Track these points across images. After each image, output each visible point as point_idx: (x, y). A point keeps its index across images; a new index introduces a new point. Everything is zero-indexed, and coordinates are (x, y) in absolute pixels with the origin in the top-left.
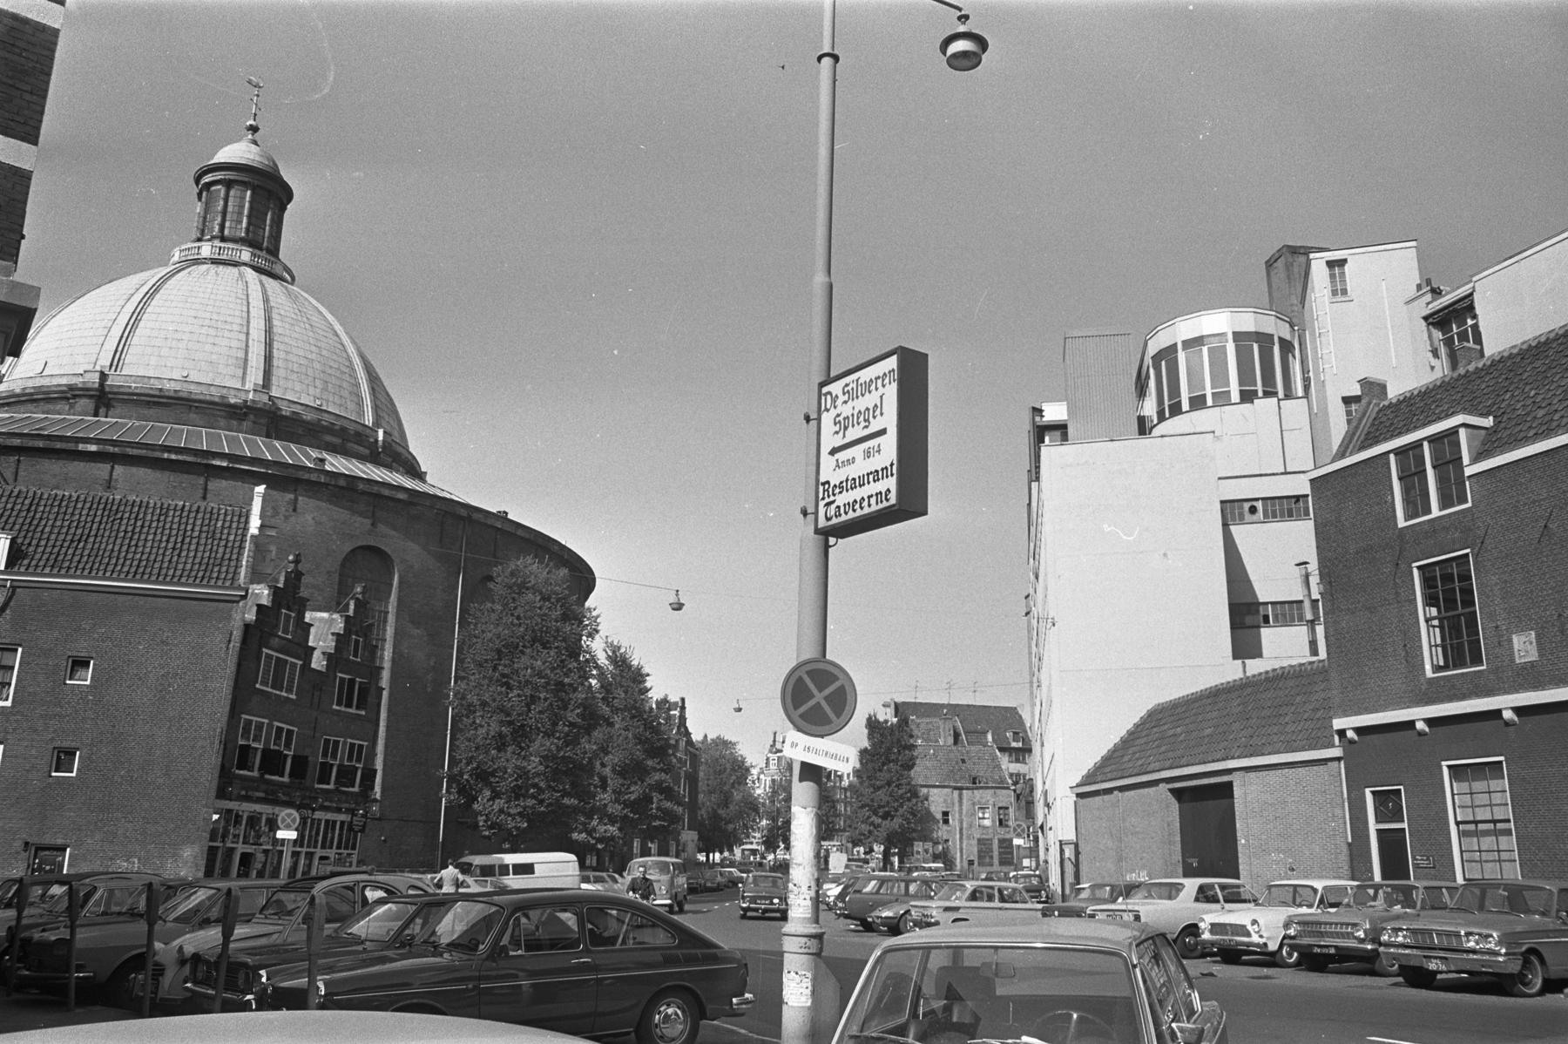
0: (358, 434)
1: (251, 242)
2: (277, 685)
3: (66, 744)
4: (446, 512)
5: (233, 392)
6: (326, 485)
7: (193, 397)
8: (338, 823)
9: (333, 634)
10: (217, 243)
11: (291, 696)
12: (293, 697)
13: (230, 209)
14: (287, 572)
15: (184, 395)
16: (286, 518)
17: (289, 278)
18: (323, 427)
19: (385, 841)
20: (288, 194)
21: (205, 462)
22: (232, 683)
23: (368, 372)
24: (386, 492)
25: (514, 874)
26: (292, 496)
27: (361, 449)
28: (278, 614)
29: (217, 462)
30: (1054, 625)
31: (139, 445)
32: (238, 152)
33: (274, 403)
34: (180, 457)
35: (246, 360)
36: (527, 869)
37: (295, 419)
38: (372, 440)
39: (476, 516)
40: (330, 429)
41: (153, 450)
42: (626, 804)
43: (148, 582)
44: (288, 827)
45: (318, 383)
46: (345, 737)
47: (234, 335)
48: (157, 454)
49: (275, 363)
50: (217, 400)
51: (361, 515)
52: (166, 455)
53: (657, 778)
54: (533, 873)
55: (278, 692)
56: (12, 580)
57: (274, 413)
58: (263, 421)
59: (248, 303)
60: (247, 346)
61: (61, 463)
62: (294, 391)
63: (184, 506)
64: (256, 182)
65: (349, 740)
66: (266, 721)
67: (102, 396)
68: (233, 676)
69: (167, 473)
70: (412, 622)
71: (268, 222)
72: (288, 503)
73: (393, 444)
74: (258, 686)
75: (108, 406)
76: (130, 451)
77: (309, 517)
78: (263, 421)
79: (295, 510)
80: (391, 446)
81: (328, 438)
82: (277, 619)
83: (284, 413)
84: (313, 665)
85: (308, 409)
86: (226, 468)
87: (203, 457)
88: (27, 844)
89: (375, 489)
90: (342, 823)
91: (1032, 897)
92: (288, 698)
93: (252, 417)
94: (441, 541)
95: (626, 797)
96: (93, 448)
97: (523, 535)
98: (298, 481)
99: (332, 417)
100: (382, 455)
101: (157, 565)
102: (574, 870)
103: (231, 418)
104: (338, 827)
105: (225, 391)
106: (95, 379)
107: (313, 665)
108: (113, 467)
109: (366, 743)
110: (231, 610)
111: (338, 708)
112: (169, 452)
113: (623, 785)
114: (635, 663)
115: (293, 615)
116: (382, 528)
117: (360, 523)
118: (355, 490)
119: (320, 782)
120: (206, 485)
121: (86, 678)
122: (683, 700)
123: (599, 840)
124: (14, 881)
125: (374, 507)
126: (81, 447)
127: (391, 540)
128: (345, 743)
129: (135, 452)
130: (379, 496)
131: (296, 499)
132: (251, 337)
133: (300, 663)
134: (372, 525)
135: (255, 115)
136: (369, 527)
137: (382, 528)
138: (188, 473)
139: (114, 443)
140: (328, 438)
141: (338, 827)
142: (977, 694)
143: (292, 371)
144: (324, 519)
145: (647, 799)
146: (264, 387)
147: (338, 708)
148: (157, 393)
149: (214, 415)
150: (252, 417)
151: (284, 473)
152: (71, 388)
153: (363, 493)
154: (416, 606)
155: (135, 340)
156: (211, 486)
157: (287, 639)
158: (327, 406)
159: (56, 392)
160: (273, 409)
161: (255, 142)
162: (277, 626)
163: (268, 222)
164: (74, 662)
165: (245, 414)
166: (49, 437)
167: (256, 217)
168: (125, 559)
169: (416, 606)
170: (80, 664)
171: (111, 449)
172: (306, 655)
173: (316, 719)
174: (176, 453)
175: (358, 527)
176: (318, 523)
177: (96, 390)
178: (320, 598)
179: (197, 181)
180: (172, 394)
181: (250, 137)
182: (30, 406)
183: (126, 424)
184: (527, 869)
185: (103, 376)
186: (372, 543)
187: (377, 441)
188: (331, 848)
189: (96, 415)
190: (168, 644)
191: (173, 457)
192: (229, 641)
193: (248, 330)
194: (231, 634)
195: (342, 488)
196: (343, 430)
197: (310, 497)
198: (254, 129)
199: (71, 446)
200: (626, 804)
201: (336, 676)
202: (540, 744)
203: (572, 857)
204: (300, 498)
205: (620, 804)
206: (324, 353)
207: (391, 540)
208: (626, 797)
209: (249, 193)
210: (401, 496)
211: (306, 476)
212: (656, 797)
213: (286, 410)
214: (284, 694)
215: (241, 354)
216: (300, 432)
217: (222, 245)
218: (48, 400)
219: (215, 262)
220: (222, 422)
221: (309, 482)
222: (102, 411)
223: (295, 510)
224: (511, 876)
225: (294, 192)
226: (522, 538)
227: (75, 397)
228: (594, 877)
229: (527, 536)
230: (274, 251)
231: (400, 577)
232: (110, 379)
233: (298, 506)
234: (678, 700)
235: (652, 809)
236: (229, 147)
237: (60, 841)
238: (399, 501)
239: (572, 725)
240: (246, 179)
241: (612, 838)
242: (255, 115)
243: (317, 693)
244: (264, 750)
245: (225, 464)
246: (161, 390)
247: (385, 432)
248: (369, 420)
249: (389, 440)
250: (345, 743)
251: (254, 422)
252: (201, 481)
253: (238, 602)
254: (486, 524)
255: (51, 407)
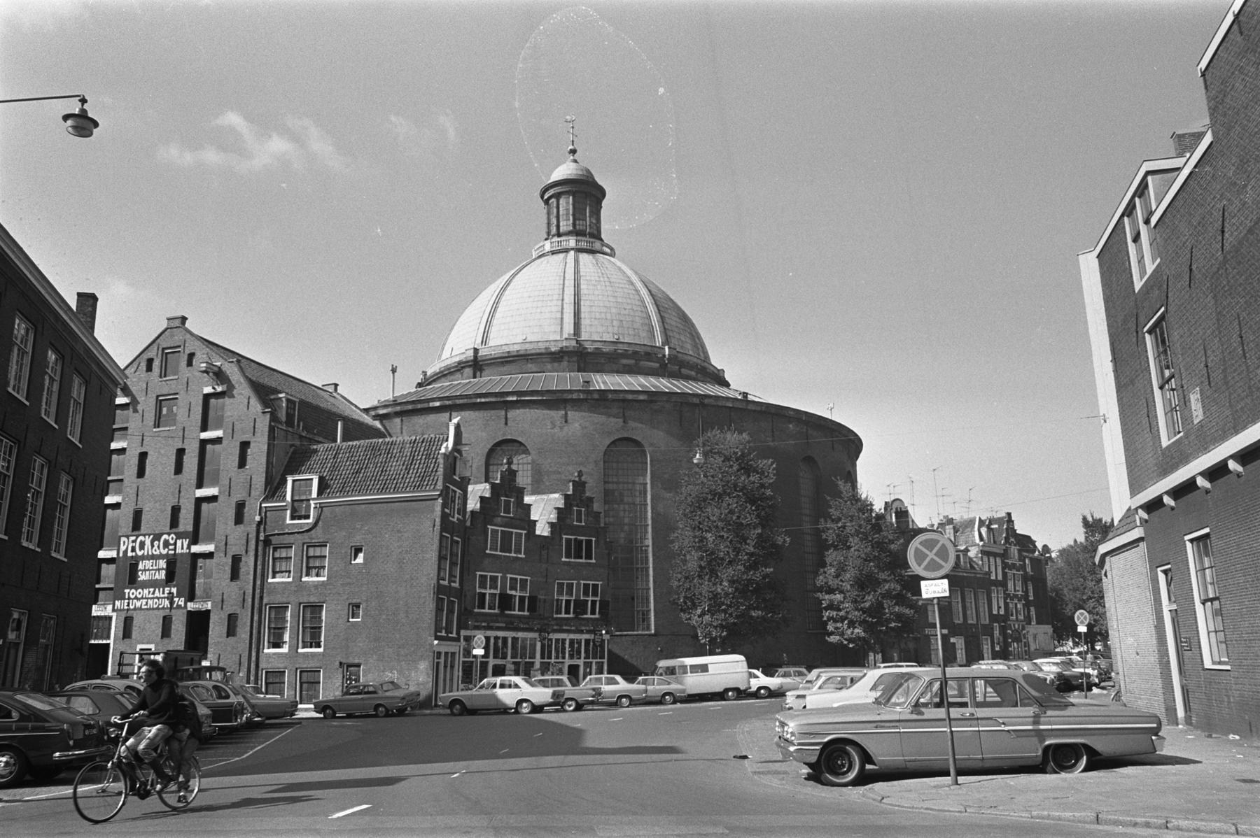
0: (647, 354)
1: (576, 232)
2: (506, 548)
3: (354, 601)
4: (682, 403)
5: (552, 343)
6: (586, 400)
7: (528, 352)
8: (567, 642)
9: (555, 508)
10: (556, 239)
11: (519, 556)
12: (522, 556)
13: (561, 213)
14: (502, 471)
15: (522, 353)
16: (561, 428)
17: (608, 250)
18: (619, 354)
19: (661, 650)
20: (602, 193)
21: (502, 399)
22: (437, 554)
23: (657, 306)
24: (630, 397)
25: (691, 672)
26: (563, 412)
27: (652, 364)
28: (498, 502)
29: (510, 398)
30: (1105, 421)
31: (461, 397)
32: (565, 170)
33: (580, 344)
34: (487, 400)
35: (562, 319)
36: (704, 668)
37: (598, 353)
38: (660, 356)
39: (706, 401)
40: (625, 355)
41: (471, 398)
42: (864, 611)
43: (390, 493)
44: (479, 647)
45: (615, 323)
46: (578, 580)
47: (555, 302)
48: (474, 401)
49: (582, 315)
50: (543, 351)
51: (614, 417)
52: (479, 400)
53: (887, 587)
54: (707, 671)
55: (508, 554)
56: (320, 503)
57: (581, 352)
58: (575, 359)
59: (564, 277)
60: (562, 309)
61: (423, 417)
62: (596, 332)
63: (416, 440)
64: (574, 189)
65: (582, 582)
66: (500, 575)
67: (476, 364)
68: (438, 549)
69: (482, 412)
70: (665, 489)
71: (588, 214)
72: (561, 417)
73: (680, 355)
74: (488, 552)
75: (481, 370)
76: (458, 402)
77: (577, 425)
78: (575, 359)
79: (566, 422)
80: (677, 357)
81: (624, 361)
82: (498, 505)
83: (589, 350)
84: (538, 532)
85: (607, 344)
86: (517, 401)
87: (501, 397)
88: (341, 663)
89: (621, 396)
90: (587, 641)
91: (375, 692)
92: (517, 558)
93: (566, 358)
94: (681, 425)
95: (862, 605)
96: (437, 404)
97: (754, 408)
98: (565, 401)
99: (625, 345)
100: (669, 365)
101: (395, 482)
102: (742, 668)
103: (554, 362)
104: (567, 646)
105: (548, 344)
106: (471, 354)
107: (538, 532)
108: (451, 414)
109: (600, 583)
110: (434, 505)
111: (567, 560)
112: (480, 397)
113: (858, 596)
114: (863, 496)
115: (512, 500)
116: (632, 424)
117: (616, 422)
118: (606, 400)
119: (557, 614)
120: (506, 415)
121: (360, 559)
122: (1009, 514)
123: (850, 640)
124: (936, 679)
125: (624, 409)
126: (431, 404)
127: (638, 430)
128: (578, 584)
129: (461, 401)
130: (624, 401)
131: (566, 414)
132: (565, 302)
133: (524, 532)
134: (624, 422)
135: (573, 141)
136: (622, 424)
137: (632, 424)
138: (480, 409)
139: (448, 398)
140: (624, 361)
141: (567, 646)
142: (956, 505)
143: (595, 319)
144: (587, 424)
145: (879, 606)
146: (574, 334)
147: (567, 560)
148: (507, 355)
149: (543, 362)
150: (566, 358)
151: (554, 397)
152: (460, 363)
153: (614, 400)
154: (666, 476)
155: (495, 322)
156: (509, 415)
157: (510, 517)
158: (624, 338)
159: (454, 367)
160: (581, 349)
161: (575, 161)
162: (499, 509)
163: (588, 214)
164: (355, 549)
165: (562, 357)
166: (413, 402)
167: (578, 214)
168: (379, 480)
169: (666, 476)
170: (358, 550)
171: (447, 403)
172: (529, 526)
173: (547, 569)
174: (484, 398)
175: (612, 425)
176: (584, 428)
177: (472, 361)
178: (591, 481)
179: (542, 197)
180: (515, 354)
181: (572, 158)
182: (443, 379)
183: (518, 377)
184: (704, 668)
185: (476, 351)
186: (626, 435)
187: (664, 356)
188: (580, 658)
189: (475, 377)
190: (401, 532)
191: (483, 400)
192: (434, 526)
193: (563, 296)
194: (435, 521)
195: (597, 400)
196: (635, 353)
197: (576, 411)
198: (573, 152)
199: (425, 405)
200: (864, 611)
201: (562, 538)
202: (727, 573)
203: (742, 658)
204: (569, 412)
205: (859, 611)
206: (620, 300)
207: (638, 430)
208: (862, 605)
209: (571, 198)
210: (642, 397)
211: (570, 397)
212: (886, 603)
213: (590, 347)
214: (513, 555)
215: (559, 315)
216: (603, 361)
217: (559, 239)
218: (451, 373)
219: (553, 253)
220: (549, 366)
221: (572, 400)
222: (478, 374)
223: (566, 422)
224: (689, 674)
225: (604, 187)
226: (755, 411)
227: (463, 368)
228: (795, 672)
229: (759, 409)
230: (597, 235)
231: (651, 457)
232: (480, 351)
233: (569, 418)
234: (1004, 515)
235: (885, 614)
236: (557, 170)
237: (356, 661)
238: (641, 401)
239: (752, 554)
240: (567, 189)
241: (859, 638)
242: (573, 141)
243: (544, 552)
244: (500, 594)
245: (515, 399)
246: (509, 352)
247: (669, 348)
248: (659, 343)
249: (674, 352)
250: (578, 584)
251: (568, 361)
252: (503, 413)
253: (437, 499)
254: (718, 406)
255: (452, 377)
